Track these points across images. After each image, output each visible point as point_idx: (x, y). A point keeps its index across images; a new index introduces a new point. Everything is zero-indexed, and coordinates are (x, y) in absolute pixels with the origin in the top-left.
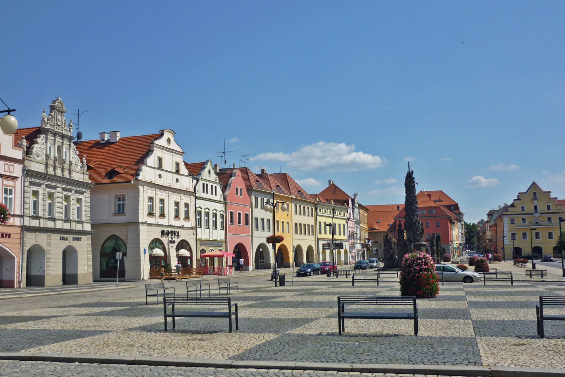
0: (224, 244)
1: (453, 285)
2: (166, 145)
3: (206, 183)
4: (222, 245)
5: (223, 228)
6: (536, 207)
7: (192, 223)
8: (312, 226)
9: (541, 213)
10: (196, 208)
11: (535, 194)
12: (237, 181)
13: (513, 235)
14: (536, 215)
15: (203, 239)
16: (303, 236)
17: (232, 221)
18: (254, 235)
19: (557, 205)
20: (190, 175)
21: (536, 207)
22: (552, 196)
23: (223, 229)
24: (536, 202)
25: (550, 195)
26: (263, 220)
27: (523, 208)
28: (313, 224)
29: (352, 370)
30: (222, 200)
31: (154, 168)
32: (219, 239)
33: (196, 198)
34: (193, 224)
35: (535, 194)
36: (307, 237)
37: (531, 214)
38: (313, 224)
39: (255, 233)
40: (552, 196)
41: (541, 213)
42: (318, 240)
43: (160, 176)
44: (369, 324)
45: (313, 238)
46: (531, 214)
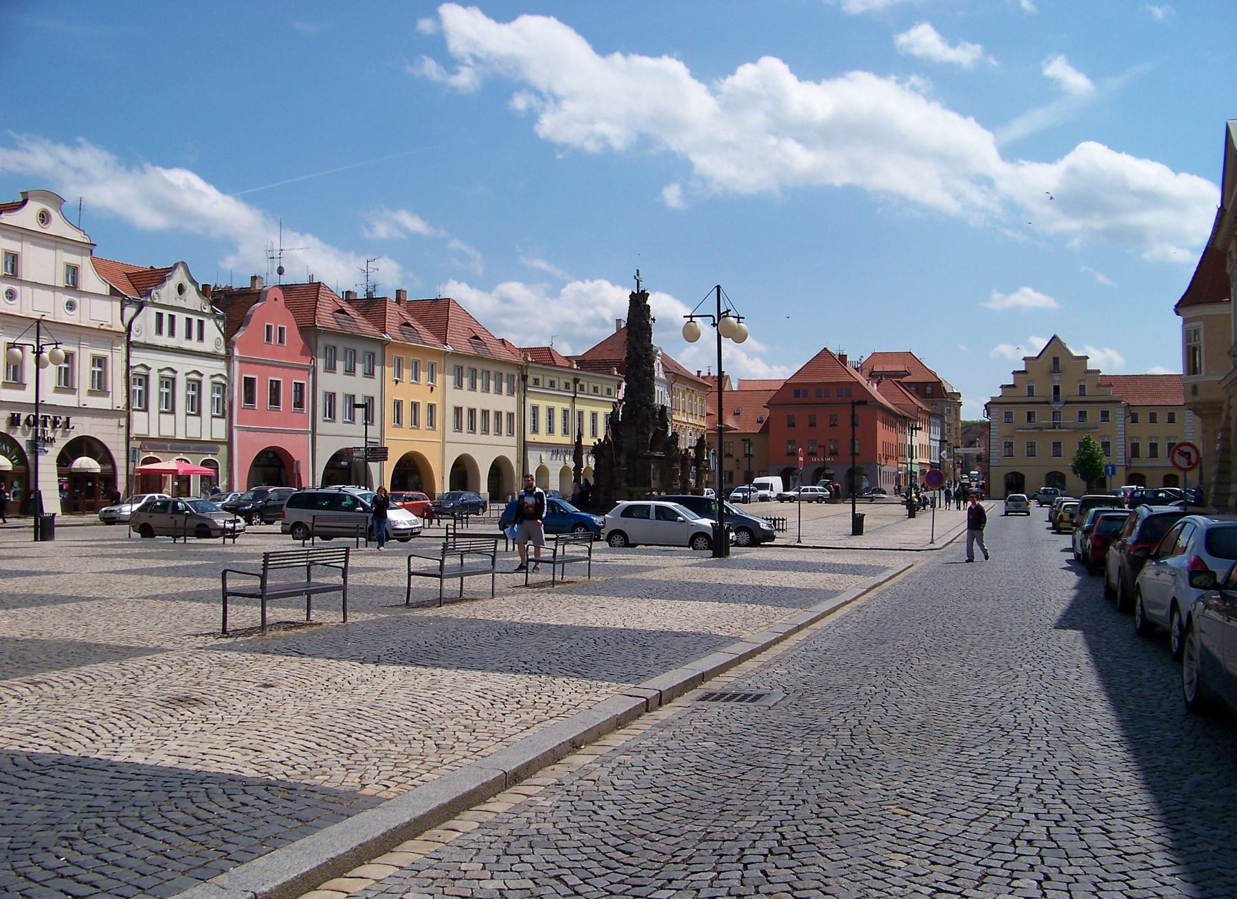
0: (223, 449)
1: (659, 553)
2: (35, 226)
3: (166, 313)
4: (218, 450)
5: (224, 411)
6: (1056, 389)
7: (117, 398)
8: (510, 415)
9: (1067, 402)
10: (128, 368)
11: (1056, 360)
12: (270, 314)
13: (1009, 446)
14: (1057, 406)
15: (154, 434)
16: (478, 437)
17: (398, 420)
18: (318, 431)
19: (1098, 386)
20: (114, 293)
21: (1056, 389)
22: (1091, 365)
23: (223, 417)
24: (1056, 377)
25: (1086, 364)
26: (415, 406)
27: (1031, 389)
28: (514, 409)
29: (855, 599)
30: (223, 352)
31: (54, 288)
32: (206, 437)
33: (130, 345)
34: (121, 403)
35: (1056, 360)
36: (491, 438)
37: (1047, 403)
38: (514, 409)
39: (322, 427)
40: (1091, 365)
41: (1067, 402)
42: (525, 446)
43: (71, 306)
44: (433, 685)
45: (513, 441)
46: (1047, 403)
